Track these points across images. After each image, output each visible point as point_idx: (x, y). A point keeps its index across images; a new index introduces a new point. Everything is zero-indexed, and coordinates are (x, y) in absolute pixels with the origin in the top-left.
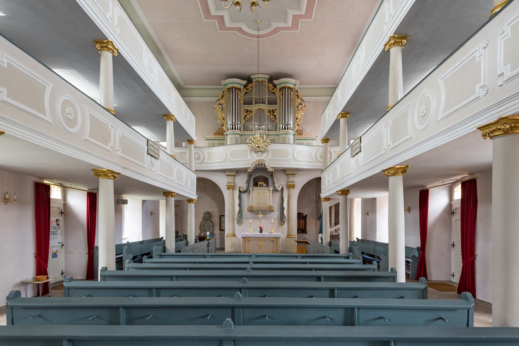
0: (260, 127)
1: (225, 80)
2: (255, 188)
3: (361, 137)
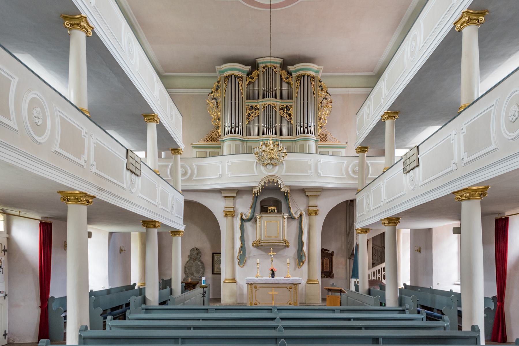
0: (269, 130)
1: (220, 65)
2: (264, 215)
3: (419, 147)
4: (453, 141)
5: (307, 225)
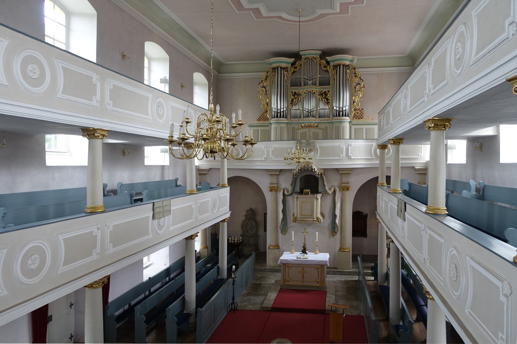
1: (268, 59)
5: (340, 199)
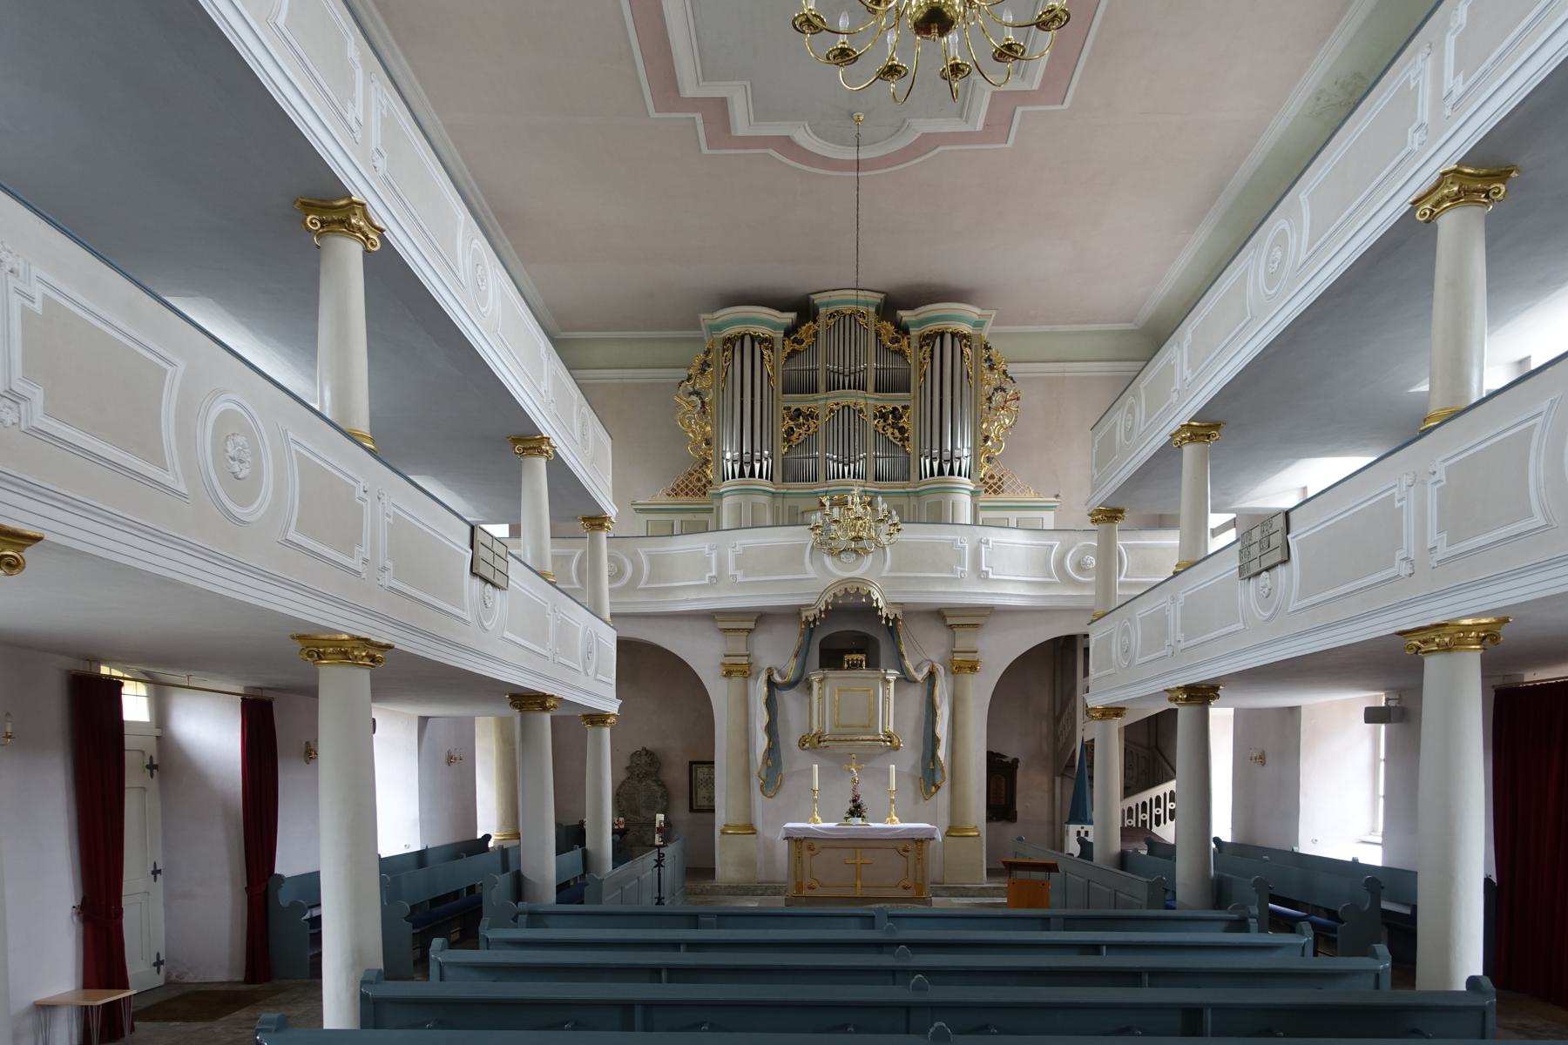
0: (846, 469)
1: (713, 311)
2: (832, 674)
3: (1292, 515)
4: (1401, 504)
